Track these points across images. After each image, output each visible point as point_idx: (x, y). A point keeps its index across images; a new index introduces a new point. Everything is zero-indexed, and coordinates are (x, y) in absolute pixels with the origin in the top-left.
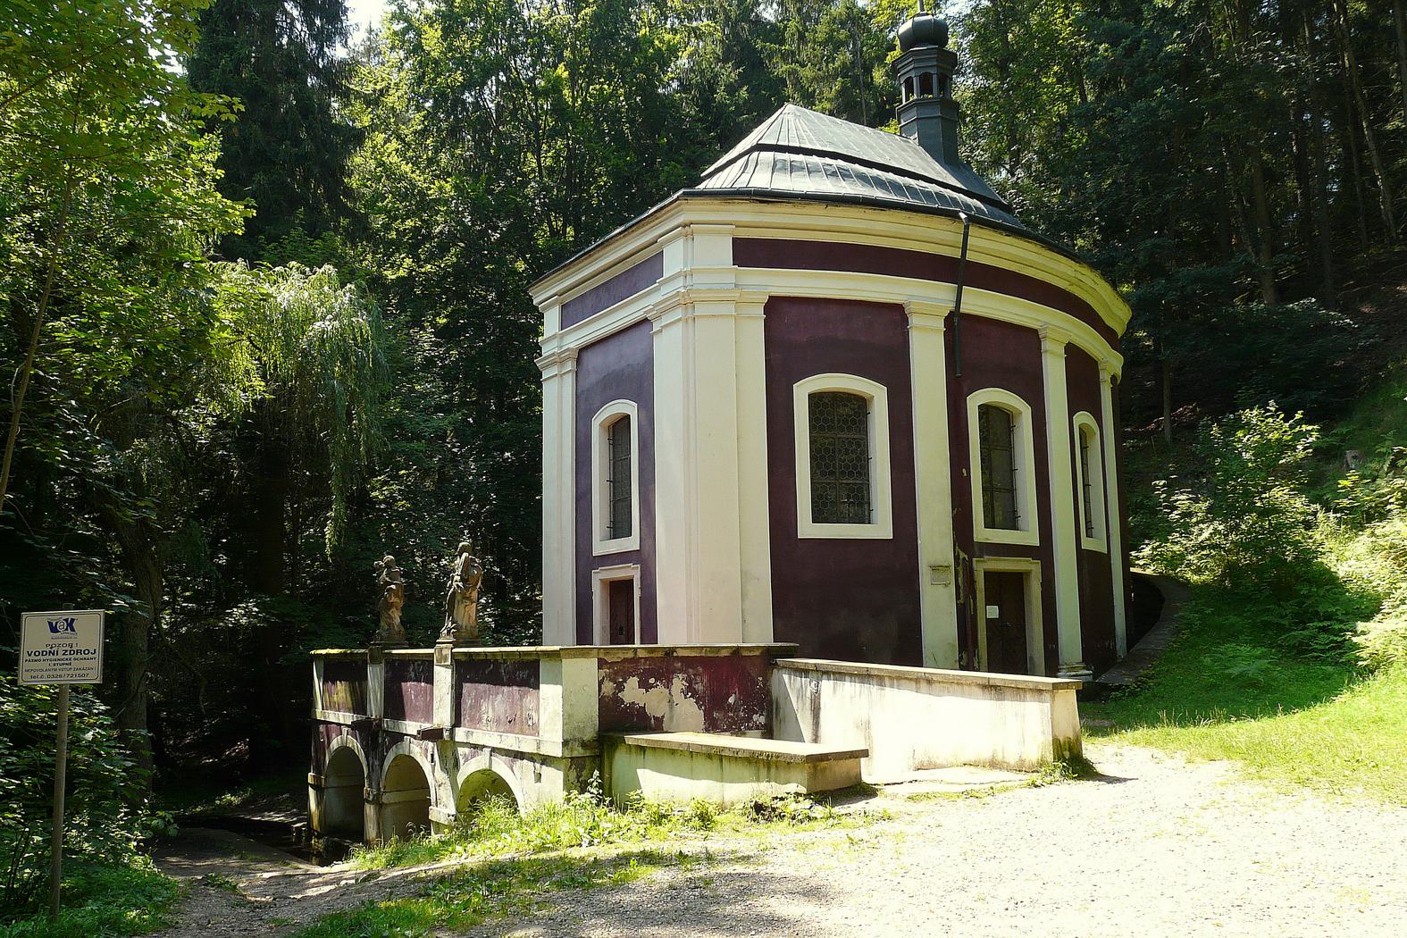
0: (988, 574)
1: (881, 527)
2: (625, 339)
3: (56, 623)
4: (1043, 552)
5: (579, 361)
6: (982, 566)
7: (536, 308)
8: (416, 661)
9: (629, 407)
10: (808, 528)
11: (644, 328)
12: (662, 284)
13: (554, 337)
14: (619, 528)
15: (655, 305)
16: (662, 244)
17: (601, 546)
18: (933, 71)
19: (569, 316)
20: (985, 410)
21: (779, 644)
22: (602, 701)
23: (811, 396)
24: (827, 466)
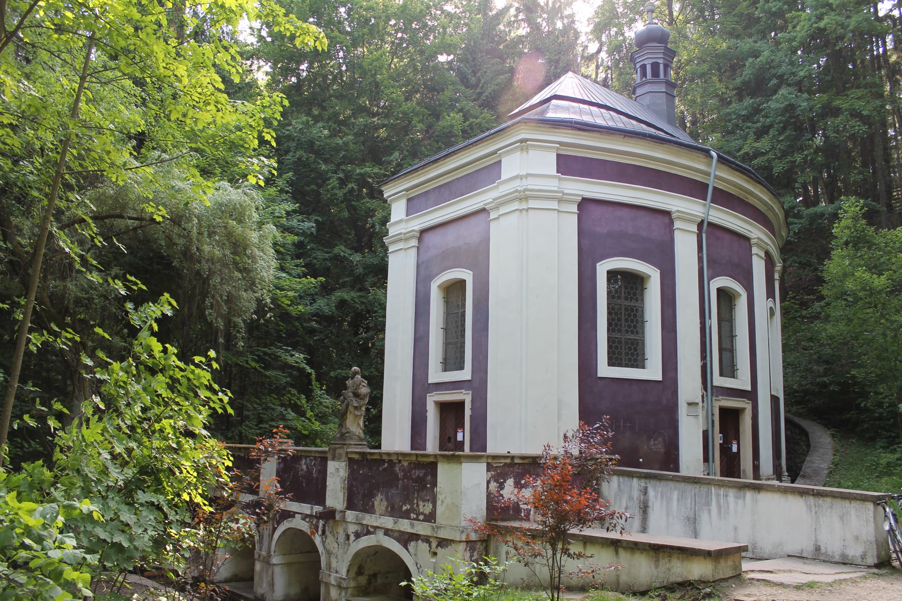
1: (653, 371)
4: (751, 395)
5: (420, 239)
7: (385, 201)
8: (309, 457)
10: (605, 370)
11: (482, 217)
12: (500, 184)
13: (401, 221)
14: (453, 360)
15: (494, 199)
16: (500, 155)
17: (436, 374)
18: (661, 61)
19: (414, 205)
20: (720, 291)
22: (489, 494)
23: (609, 272)
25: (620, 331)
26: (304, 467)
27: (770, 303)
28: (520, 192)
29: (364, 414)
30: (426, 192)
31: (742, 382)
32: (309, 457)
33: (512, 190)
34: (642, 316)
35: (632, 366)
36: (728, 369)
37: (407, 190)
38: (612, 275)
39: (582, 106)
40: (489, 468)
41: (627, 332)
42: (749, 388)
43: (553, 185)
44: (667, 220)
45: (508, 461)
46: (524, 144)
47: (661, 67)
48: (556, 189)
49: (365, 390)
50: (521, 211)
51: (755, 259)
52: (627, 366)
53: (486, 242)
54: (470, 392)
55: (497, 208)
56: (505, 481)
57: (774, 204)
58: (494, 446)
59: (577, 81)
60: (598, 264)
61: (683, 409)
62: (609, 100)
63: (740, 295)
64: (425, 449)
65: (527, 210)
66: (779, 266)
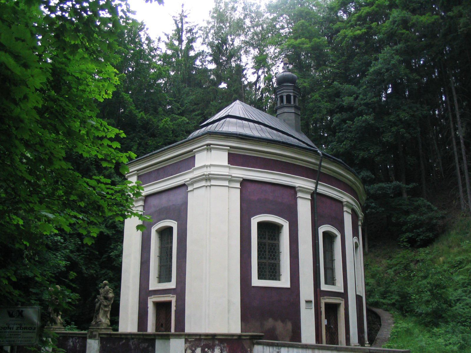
0: (327, 304)
1: (284, 282)
2: (172, 193)
3: (13, 312)
4: (344, 295)
6: (324, 301)
8: (74, 337)
9: (173, 224)
10: (256, 282)
11: (183, 189)
15: (191, 179)
18: (291, 94)
20: (325, 234)
21: (141, 333)
24: (263, 255)
25: (265, 258)
26: (71, 344)
27: (355, 240)
28: (206, 175)
29: (110, 309)
30: (149, 172)
31: (339, 287)
32: (74, 337)
33: (202, 174)
34: (279, 249)
35: (273, 279)
36: (330, 280)
37: (138, 170)
38: (261, 225)
39: (244, 122)
40: (186, 341)
41: (269, 258)
42: (342, 291)
43: (225, 171)
44: (293, 192)
45: (198, 337)
46: (209, 147)
47: (292, 97)
48: (227, 174)
49: (111, 295)
50: (206, 186)
51: (345, 214)
52: (269, 279)
53: (185, 204)
54: (175, 296)
55: (192, 184)
56: (195, 349)
57: (357, 181)
58: (189, 329)
59: (241, 106)
60: (252, 219)
61: (303, 304)
62: (261, 118)
63: (337, 236)
64: (146, 330)
65: (210, 186)
66: (361, 215)
